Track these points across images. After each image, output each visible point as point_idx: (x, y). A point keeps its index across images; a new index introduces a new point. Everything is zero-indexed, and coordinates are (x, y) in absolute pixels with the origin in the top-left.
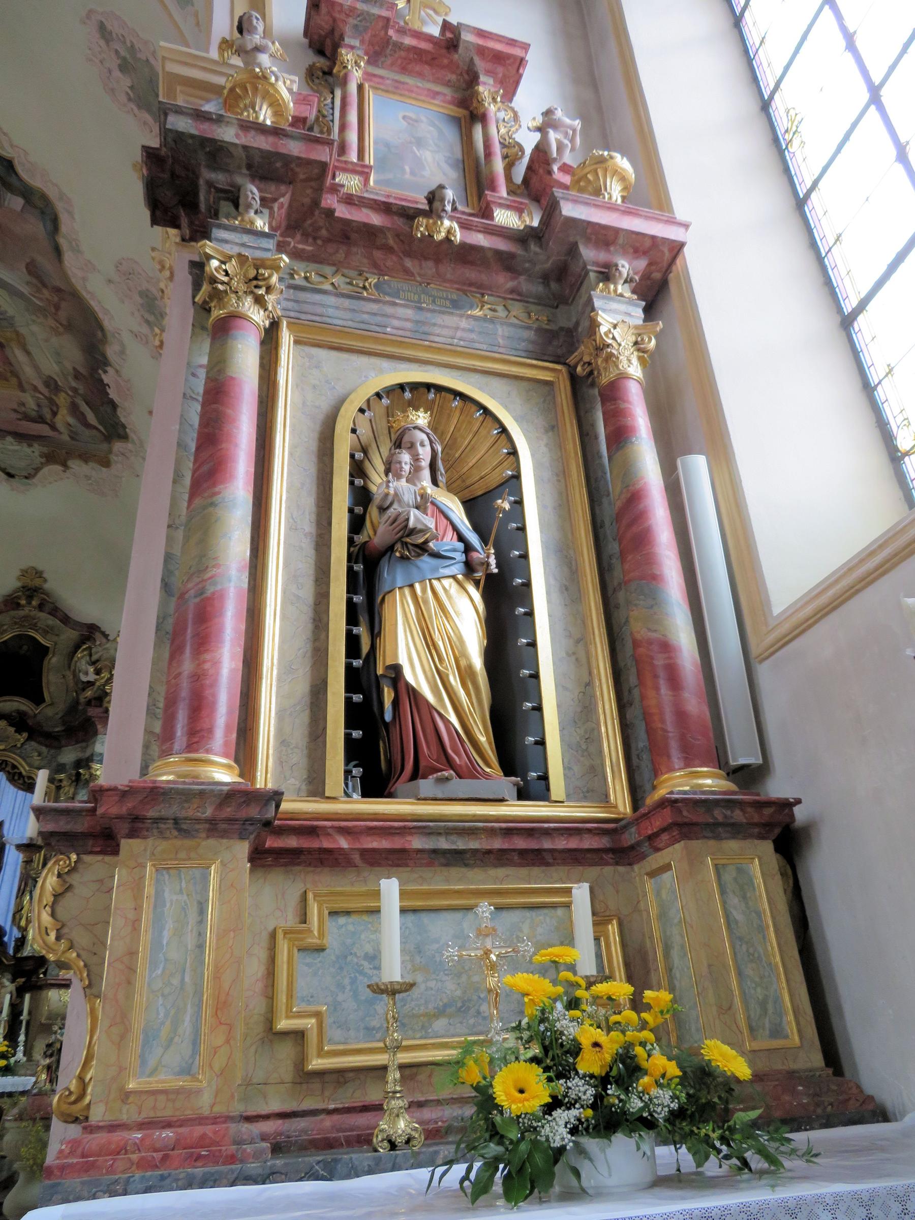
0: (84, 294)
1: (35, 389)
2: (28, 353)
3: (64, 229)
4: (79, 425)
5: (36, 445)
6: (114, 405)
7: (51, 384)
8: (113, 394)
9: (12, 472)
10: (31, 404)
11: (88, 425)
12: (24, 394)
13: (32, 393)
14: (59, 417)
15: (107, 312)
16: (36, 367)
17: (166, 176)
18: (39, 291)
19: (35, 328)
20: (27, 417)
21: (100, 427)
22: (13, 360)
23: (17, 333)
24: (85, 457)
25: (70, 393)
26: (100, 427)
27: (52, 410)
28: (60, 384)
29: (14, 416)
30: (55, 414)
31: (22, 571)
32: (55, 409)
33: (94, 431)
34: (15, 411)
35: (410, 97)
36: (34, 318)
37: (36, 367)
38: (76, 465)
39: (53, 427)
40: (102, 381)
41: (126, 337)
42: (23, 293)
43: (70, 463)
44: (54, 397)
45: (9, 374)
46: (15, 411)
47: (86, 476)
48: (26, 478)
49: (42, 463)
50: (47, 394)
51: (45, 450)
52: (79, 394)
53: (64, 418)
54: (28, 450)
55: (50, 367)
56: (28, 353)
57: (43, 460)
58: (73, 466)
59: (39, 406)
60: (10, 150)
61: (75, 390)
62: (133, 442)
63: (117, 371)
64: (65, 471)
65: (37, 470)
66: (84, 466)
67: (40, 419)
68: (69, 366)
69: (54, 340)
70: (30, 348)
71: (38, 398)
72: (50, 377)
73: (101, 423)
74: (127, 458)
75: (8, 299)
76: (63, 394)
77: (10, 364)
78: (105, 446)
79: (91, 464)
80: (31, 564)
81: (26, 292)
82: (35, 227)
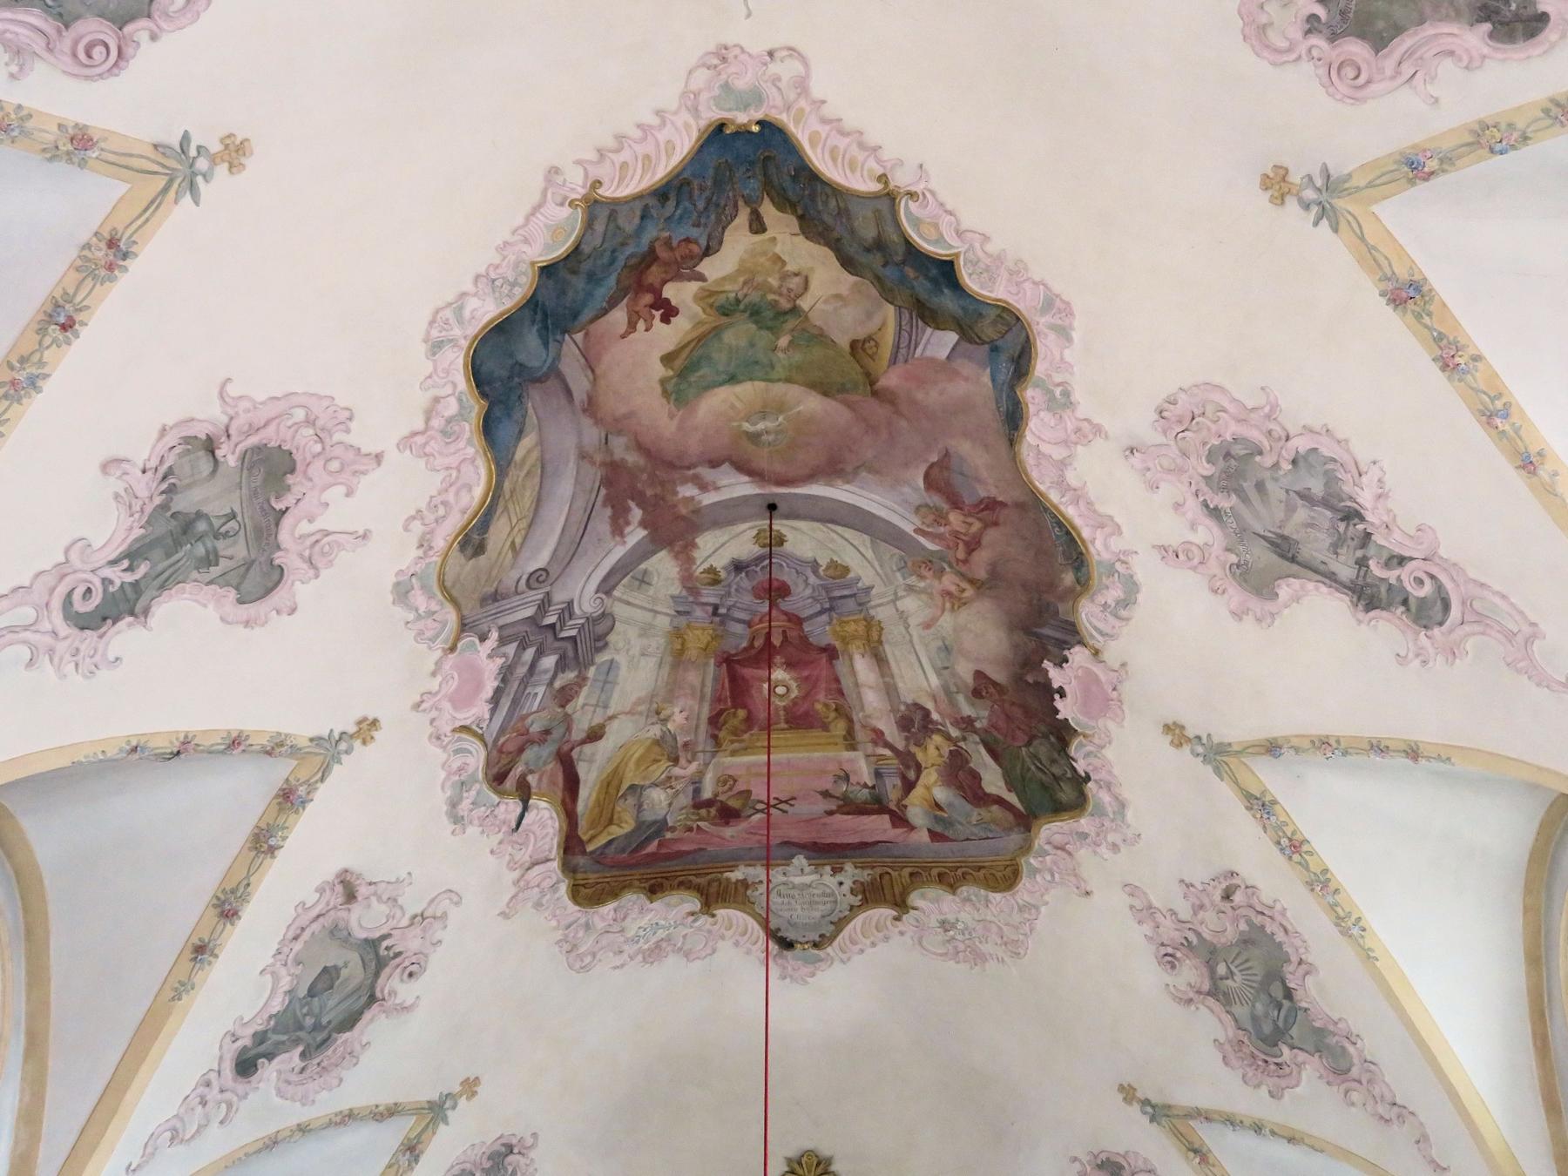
0: (1054, 496)
1: (878, 737)
2: (880, 660)
3: (1040, 368)
4: (960, 802)
5: (849, 867)
6: (1063, 734)
7: (916, 722)
8: (1066, 709)
9: (790, 935)
10: (864, 772)
11: (979, 797)
12: (851, 754)
13: (870, 748)
14: (918, 791)
15: (1105, 523)
16: (890, 690)
17: (1043, 320)
18: (940, 518)
19: (910, 604)
20: (849, 807)
21: (1012, 798)
22: (846, 683)
23: (869, 622)
24: (950, 879)
25: (954, 733)
26: (1012, 798)
27: (904, 778)
28: (935, 716)
29: (823, 805)
30: (909, 786)
31: (789, 1161)
32: (912, 775)
33: (995, 808)
34: (826, 794)
35: (559, 543)
36: (913, 580)
37: (890, 690)
38: (930, 903)
39: (899, 820)
40: (1048, 683)
41: (1145, 567)
42: (902, 533)
43: (915, 899)
44: (913, 749)
45: (833, 715)
46: (826, 794)
47: (943, 923)
48: (816, 945)
49: (852, 908)
50: (900, 745)
51: (865, 876)
52: (975, 731)
53: (933, 787)
54: (830, 881)
55: (919, 680)
56: (880, 660)
57: (856, 901)
58: (919, 903)
59: (878, 774)
60: (954, 241)
61: (967, 724)
62: (1100, 812)
63: (1096, 653)
64: (897, 919)
65: (840, 924)
66: (947, 898)
67: (877, 805)
68: (965, 670)
69: (947, 622)
70: (889, 651)
71: (882, 757)
72: (917, 706)
73: (1011, 786)
74: (1070, 854)
75: (869, 554)
76: (937, 739)
77: (841, 693)
78: (1016, 838)
79: (964, 890)
80: (809, 1145)
81: (908, 528)
82: (976, 383)
